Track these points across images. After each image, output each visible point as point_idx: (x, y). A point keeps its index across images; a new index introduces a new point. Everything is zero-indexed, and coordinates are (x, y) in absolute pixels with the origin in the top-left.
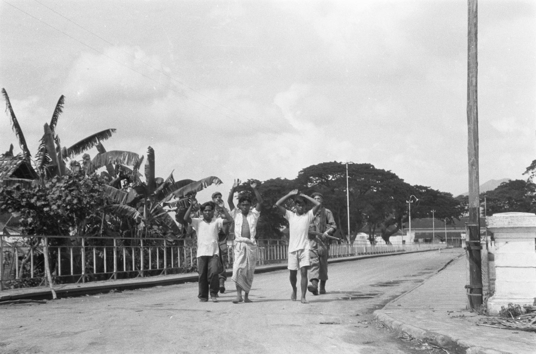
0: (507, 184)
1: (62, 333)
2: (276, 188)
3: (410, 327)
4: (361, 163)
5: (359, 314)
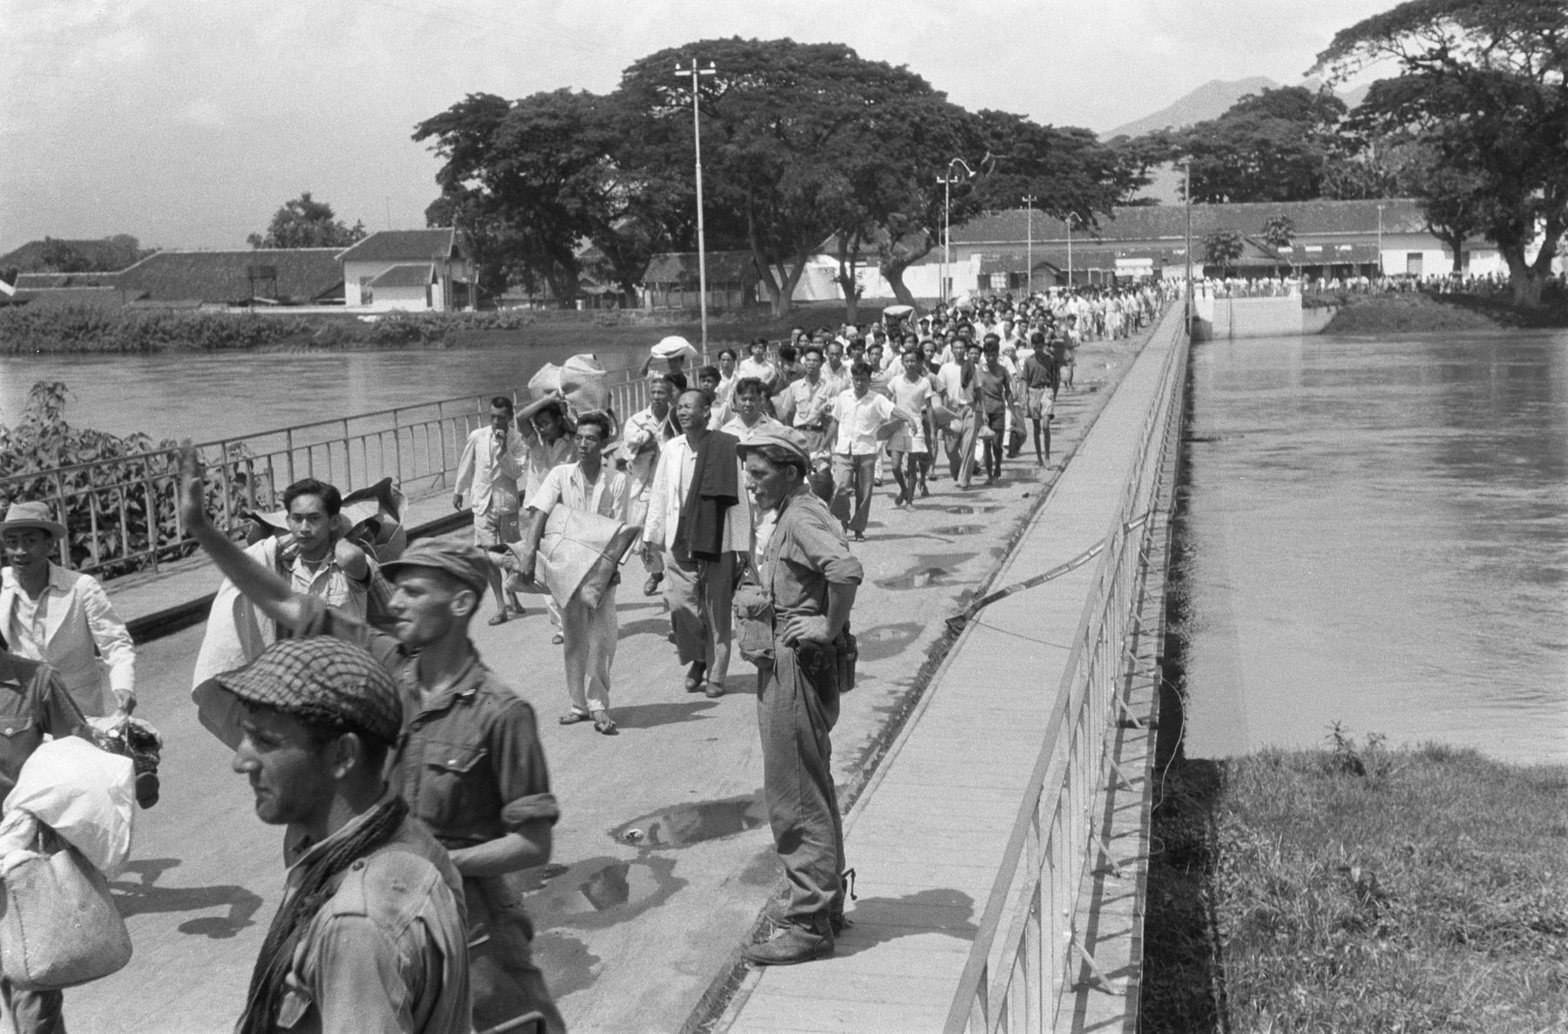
0: (1256, 99)
2: (555, 123)
4: (818, 42)
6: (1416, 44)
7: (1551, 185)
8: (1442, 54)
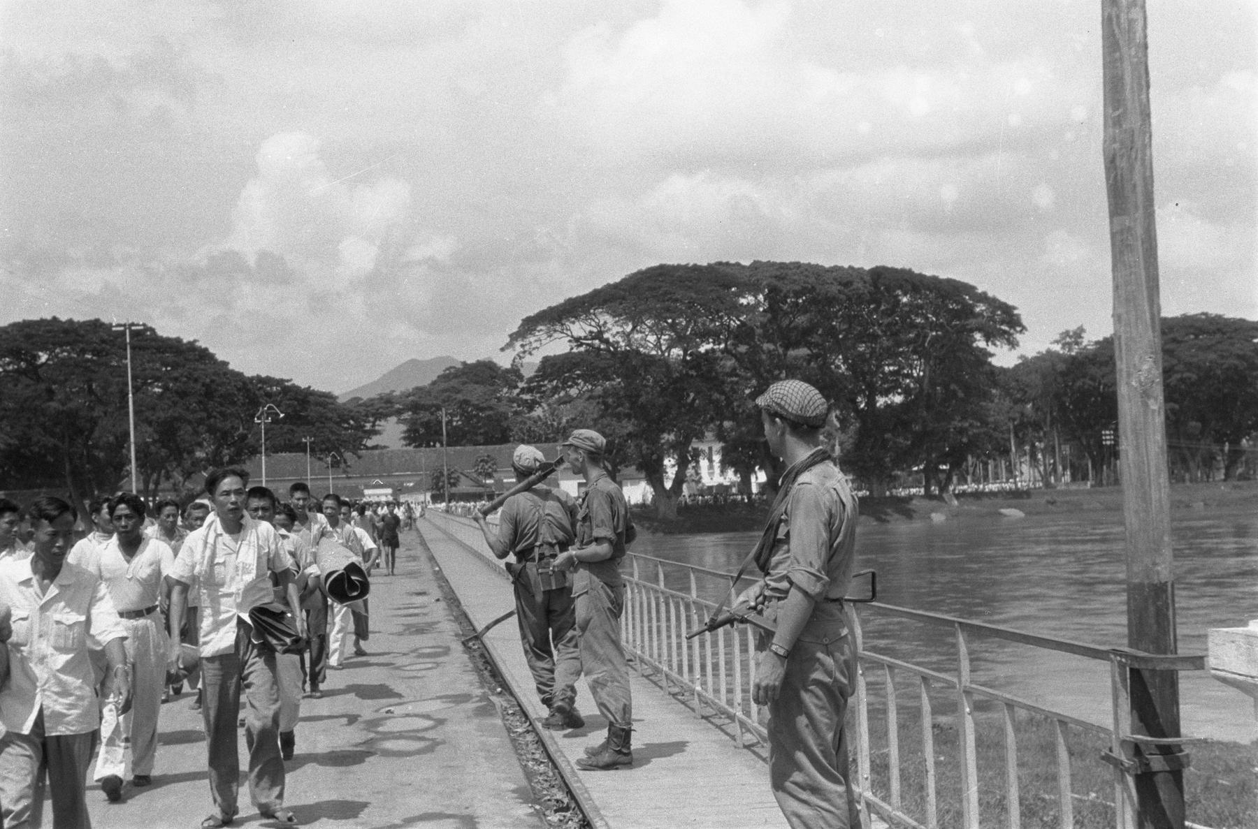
6: (579, 328)
7: (679, 430)
8: (599, 335)
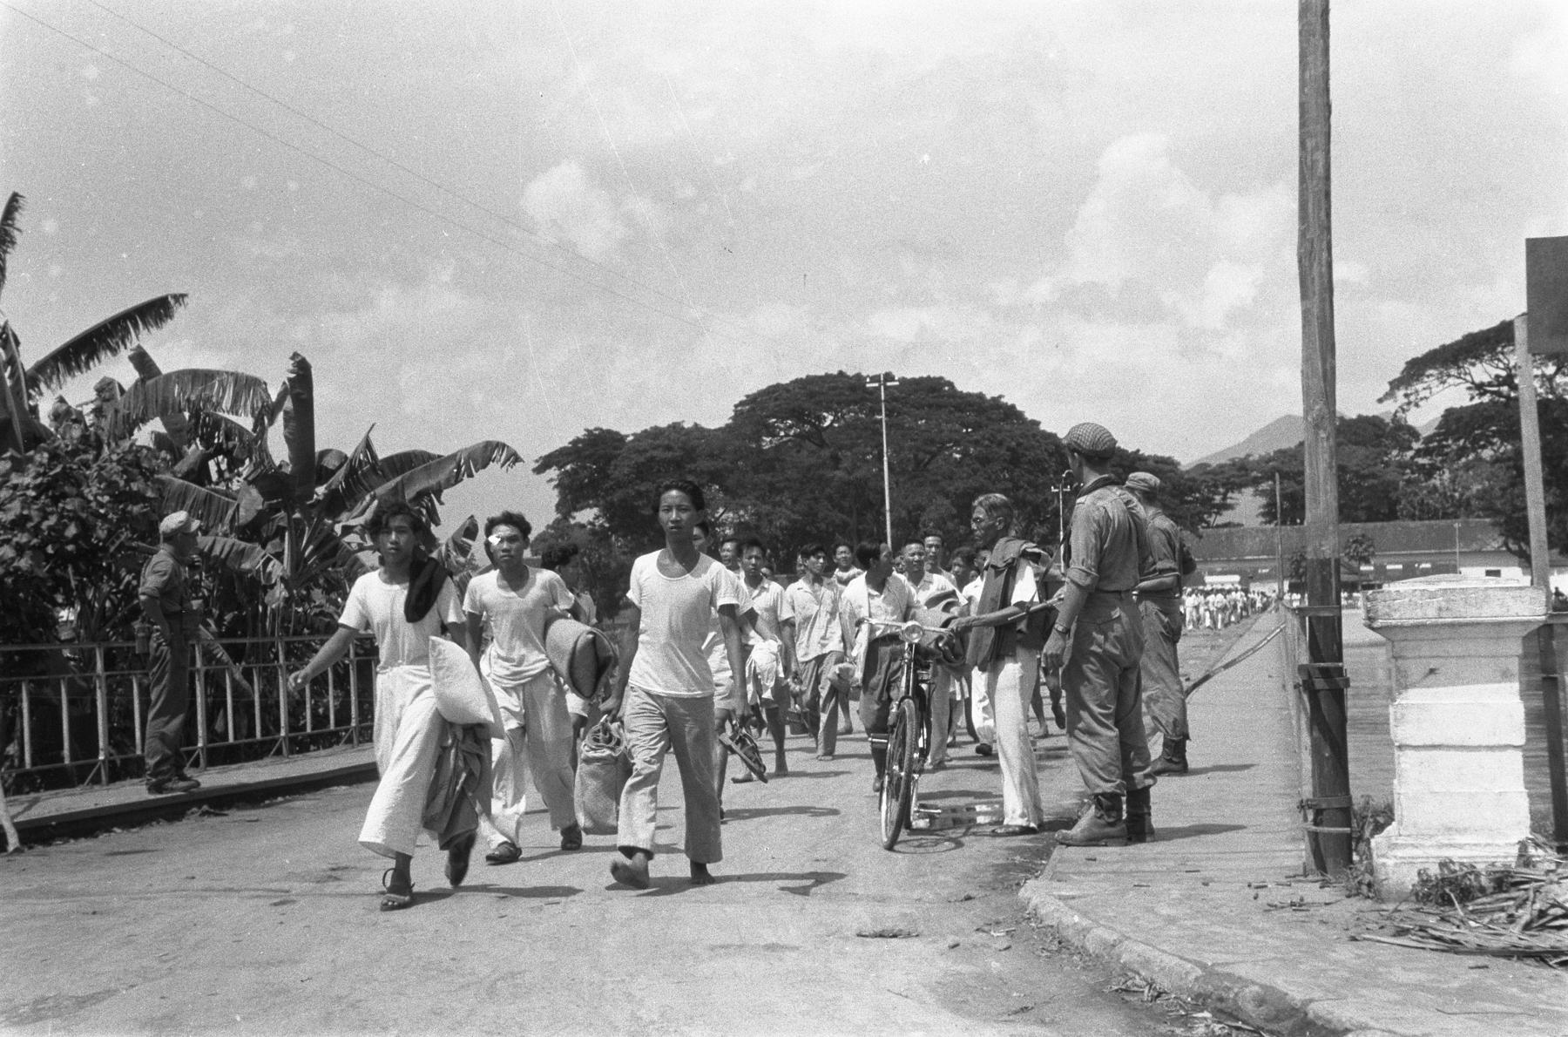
1: (36, 1002)
2: (669, 455)
3: (1150, 953)
4: (917, 376)
5: (973, 893)
6: (1482, 372)
